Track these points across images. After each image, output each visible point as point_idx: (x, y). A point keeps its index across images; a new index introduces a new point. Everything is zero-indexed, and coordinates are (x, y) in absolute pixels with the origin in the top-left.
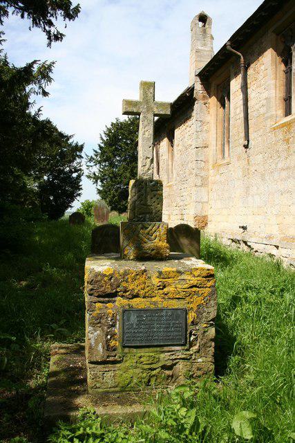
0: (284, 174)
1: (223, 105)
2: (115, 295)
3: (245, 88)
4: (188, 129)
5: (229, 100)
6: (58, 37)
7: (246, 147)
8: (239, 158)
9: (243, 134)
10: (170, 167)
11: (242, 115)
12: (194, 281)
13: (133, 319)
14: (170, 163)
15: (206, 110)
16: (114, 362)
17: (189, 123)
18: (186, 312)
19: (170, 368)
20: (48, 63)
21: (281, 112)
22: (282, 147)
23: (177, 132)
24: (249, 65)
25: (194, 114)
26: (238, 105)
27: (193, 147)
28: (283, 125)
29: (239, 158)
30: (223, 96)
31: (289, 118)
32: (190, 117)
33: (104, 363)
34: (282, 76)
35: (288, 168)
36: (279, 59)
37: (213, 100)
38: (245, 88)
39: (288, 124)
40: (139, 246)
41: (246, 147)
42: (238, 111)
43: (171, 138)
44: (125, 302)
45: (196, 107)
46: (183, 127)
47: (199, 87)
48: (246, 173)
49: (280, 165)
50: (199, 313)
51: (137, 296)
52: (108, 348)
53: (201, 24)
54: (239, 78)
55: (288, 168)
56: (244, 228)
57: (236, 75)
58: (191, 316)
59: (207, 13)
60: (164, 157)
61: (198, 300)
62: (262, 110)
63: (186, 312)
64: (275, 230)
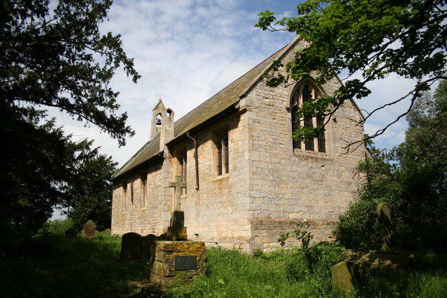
0: (219, 205)
1: (182, 164)
2: (172, 252)
3: (196, 156)
4: (159, 175)
5: (186, 161)
6: (123, 144)
7: (197, 189)
8: (193, 196)
9: (195, 182)
10: (142, 198)
11: (195, 171)
12: (199, 246)
13: (179, 259)
14: (142, 195)
15: (171, 167)
16: (173, 276)
17: (159, 172)
18: (196, 257)
19: (191, 278)
20: (89, 141)
21: (216, 173)
22: (218, 191)
23: (149, 176)
24: (199, 146)
25: (163, 167)
26: (192, 169)
27: (162, 187)
28: (218, 180)
29: (193, 196)
30: (182, 159)
31: (220, 177)
32: (160, 168)
33: (169, 276)
34: (217, 155)
35: (221, 202)
36: (215, 146)
37: (175, 160)
38: (196, 156)
39: (221, 180)
40: (177, 235)
41: (197, 189)
42: (192, 169)
43: (144, 179)
44: (176, 254)
45: (165, 162)
46: (154, 174)
47: (166, 151)
48: (197, 204)
49: (217, 201)
50: (200, 258)
51: (180, 252)
52: (171, 271)
53: (168, 114)
54: (193, 150)
55: (221, 202)
56: (197, 235)
57: (191, 149)
58: (198, 258)
59: (171, 109)
60: (137, 191)
61: (200, 253)
62: (207, 171)
63: (196, 257)
64: (215, 234)
